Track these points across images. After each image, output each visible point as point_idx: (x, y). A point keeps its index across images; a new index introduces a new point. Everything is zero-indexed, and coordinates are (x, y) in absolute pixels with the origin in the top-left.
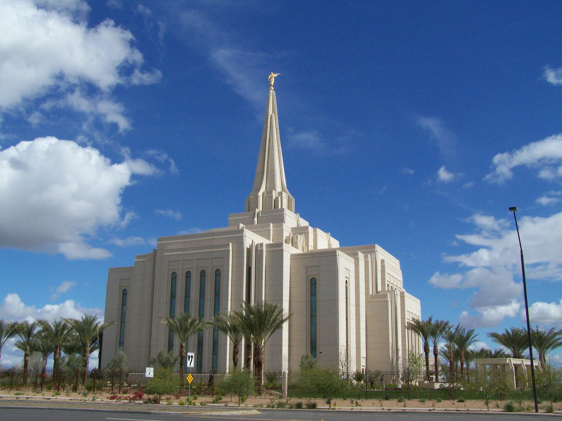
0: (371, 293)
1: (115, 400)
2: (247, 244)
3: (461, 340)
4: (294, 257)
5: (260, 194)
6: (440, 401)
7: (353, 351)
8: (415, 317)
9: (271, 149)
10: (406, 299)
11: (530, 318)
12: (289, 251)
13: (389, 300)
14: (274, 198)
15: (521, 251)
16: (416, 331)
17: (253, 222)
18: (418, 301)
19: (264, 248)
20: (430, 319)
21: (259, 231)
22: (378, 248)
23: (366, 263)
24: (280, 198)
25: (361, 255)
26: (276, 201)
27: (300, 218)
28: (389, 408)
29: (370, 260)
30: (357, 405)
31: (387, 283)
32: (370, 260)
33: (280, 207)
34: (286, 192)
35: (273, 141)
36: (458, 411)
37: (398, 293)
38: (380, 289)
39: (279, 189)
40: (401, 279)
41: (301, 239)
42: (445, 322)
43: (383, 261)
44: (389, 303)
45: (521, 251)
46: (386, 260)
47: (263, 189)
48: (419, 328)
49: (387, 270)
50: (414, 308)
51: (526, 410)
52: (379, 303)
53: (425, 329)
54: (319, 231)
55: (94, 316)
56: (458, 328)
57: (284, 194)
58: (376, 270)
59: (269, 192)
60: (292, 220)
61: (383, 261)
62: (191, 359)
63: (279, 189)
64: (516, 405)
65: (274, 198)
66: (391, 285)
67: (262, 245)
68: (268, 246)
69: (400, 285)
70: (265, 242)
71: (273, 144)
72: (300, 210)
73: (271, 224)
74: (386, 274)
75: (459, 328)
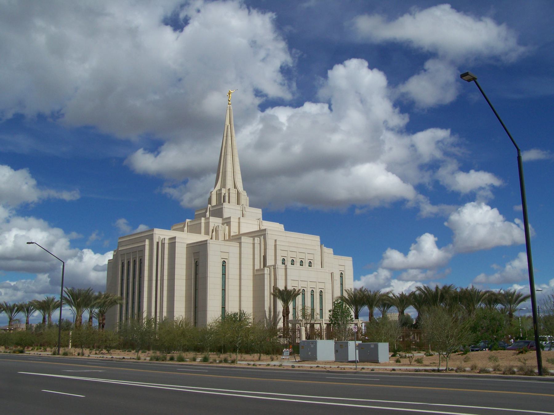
14: (223, 195)
24: (227, 195)
26: (224, 197)
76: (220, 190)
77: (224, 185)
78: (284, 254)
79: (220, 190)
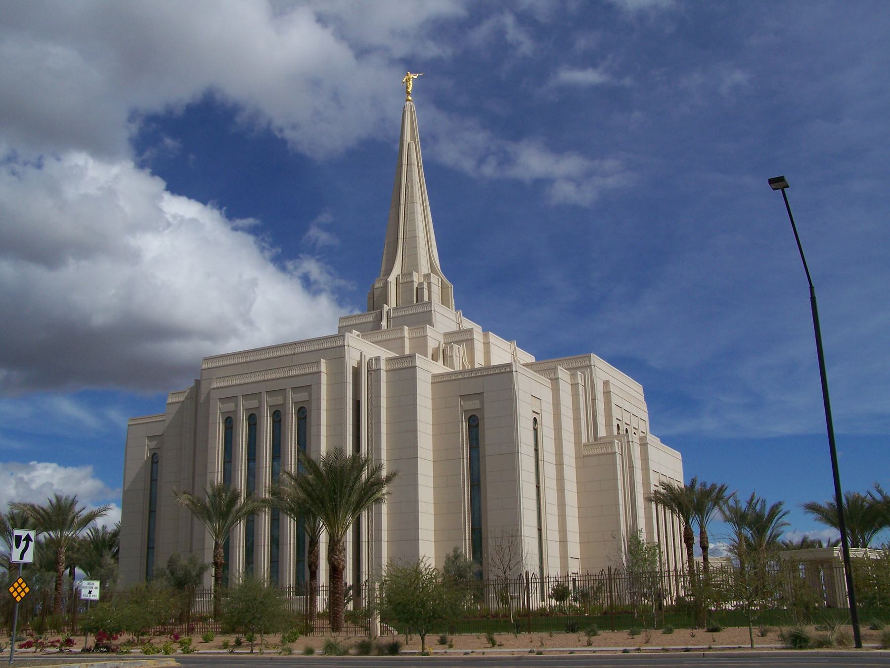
0: (584, 440)
1: (33, 649)
2: (352, 360)
3: (756, 523)
4: (438, 381)
5: (392, 279)
6: (670, 631)
7: (553, 543)
8: (664, 479)
9: (410, 202)
10: (651, 451)
11: (836, 431)
12: (428, 369)
13: (617, 450)
14: (416, 285)
15: (811, 288)
16: (666, 505)
17: (379, 327)
18: (678, 455)
19: (383, 366)
20: (693, 482)
21: (385, 341)
22: (596, 360)
23: (574, 386)
24: (425, 286)
25: (563, 374)
26: (420, 290)
27: (518, 349)
28: (623, 648)
29: (580, 381)
30: (494, 644)
31: (615, 423)
32: (580, 381)
33: (426, 299)
34: (437, 275)
35: (412, 187)
36: (667, 650)
37: (635, 439)
38: (602, 432)
39: (425, 268)
40: (646, 417)
41: (459, 353)
42: (719, 486)
43: (606, 383)
44: (618, 457)
45: (811, 288)
46: (612, 381)
47: (397, 270)
48: (671, 499)
49: (615, 400)
50: (668, 467)
51: (835, 644)
52: (600, 461)
53: (688, 503)
54: (493, 338)
55: (71, 498)
56: (752, 499)
57: (434, 279)
58: (594, 399)
59: (407, 274)
60: (446, 319)
61: (606, 383)
62: (23, 544)
63: (425, 268)
64: (811, 630)
65: (416, 285)
66: (623, 427)
67: (378, 359)
68: (389, 360)
69: (645, 427)
70: (385, 354)
71: (412, 192)
72: (466, 304)
73: (406, 327)
74: (614, 406)
75: (754, 501)
77: (411, 265)
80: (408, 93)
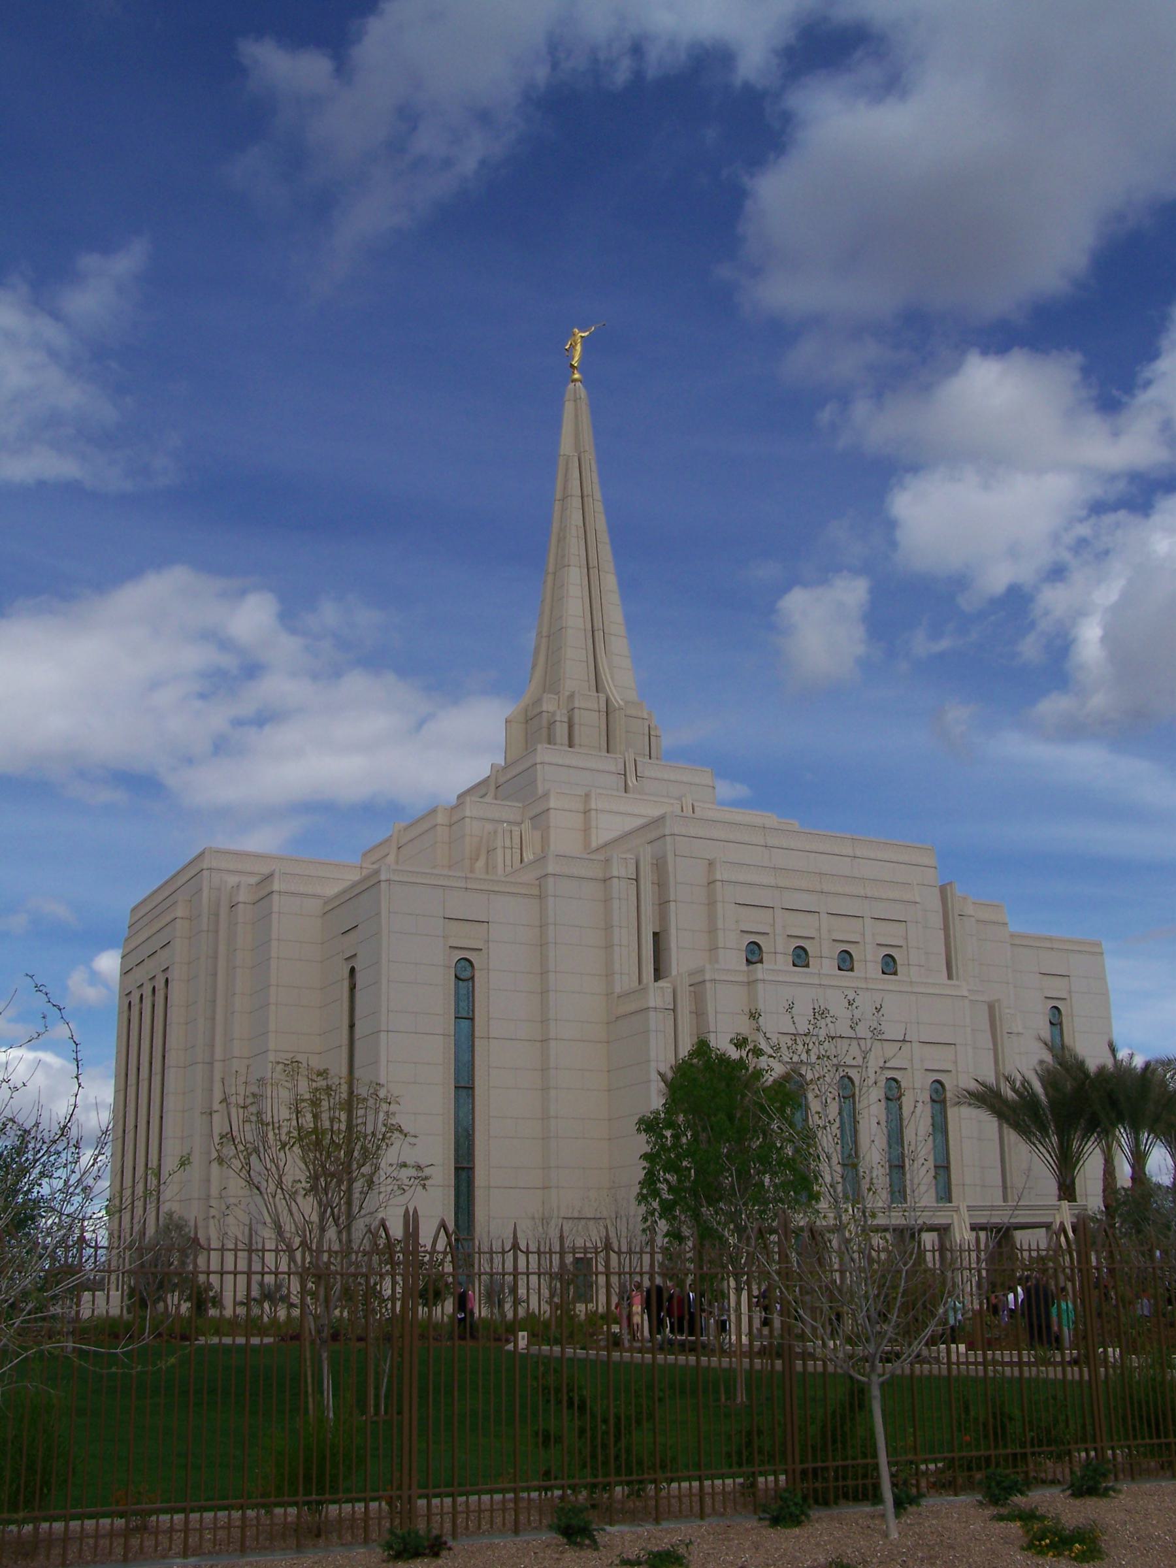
24: (562, 716)
76: (538, 701)
78: (755, 921)
79: (538, 701)
80: (572, 366)
